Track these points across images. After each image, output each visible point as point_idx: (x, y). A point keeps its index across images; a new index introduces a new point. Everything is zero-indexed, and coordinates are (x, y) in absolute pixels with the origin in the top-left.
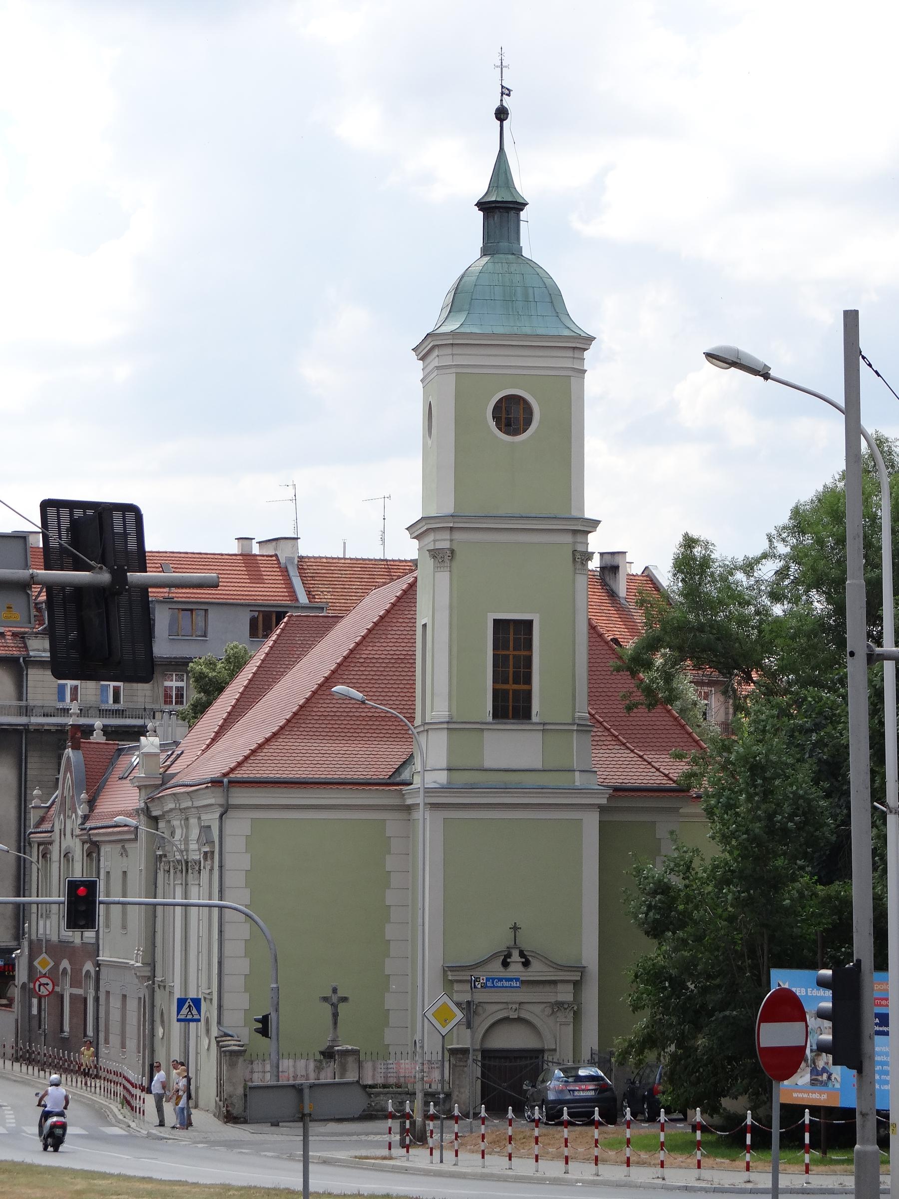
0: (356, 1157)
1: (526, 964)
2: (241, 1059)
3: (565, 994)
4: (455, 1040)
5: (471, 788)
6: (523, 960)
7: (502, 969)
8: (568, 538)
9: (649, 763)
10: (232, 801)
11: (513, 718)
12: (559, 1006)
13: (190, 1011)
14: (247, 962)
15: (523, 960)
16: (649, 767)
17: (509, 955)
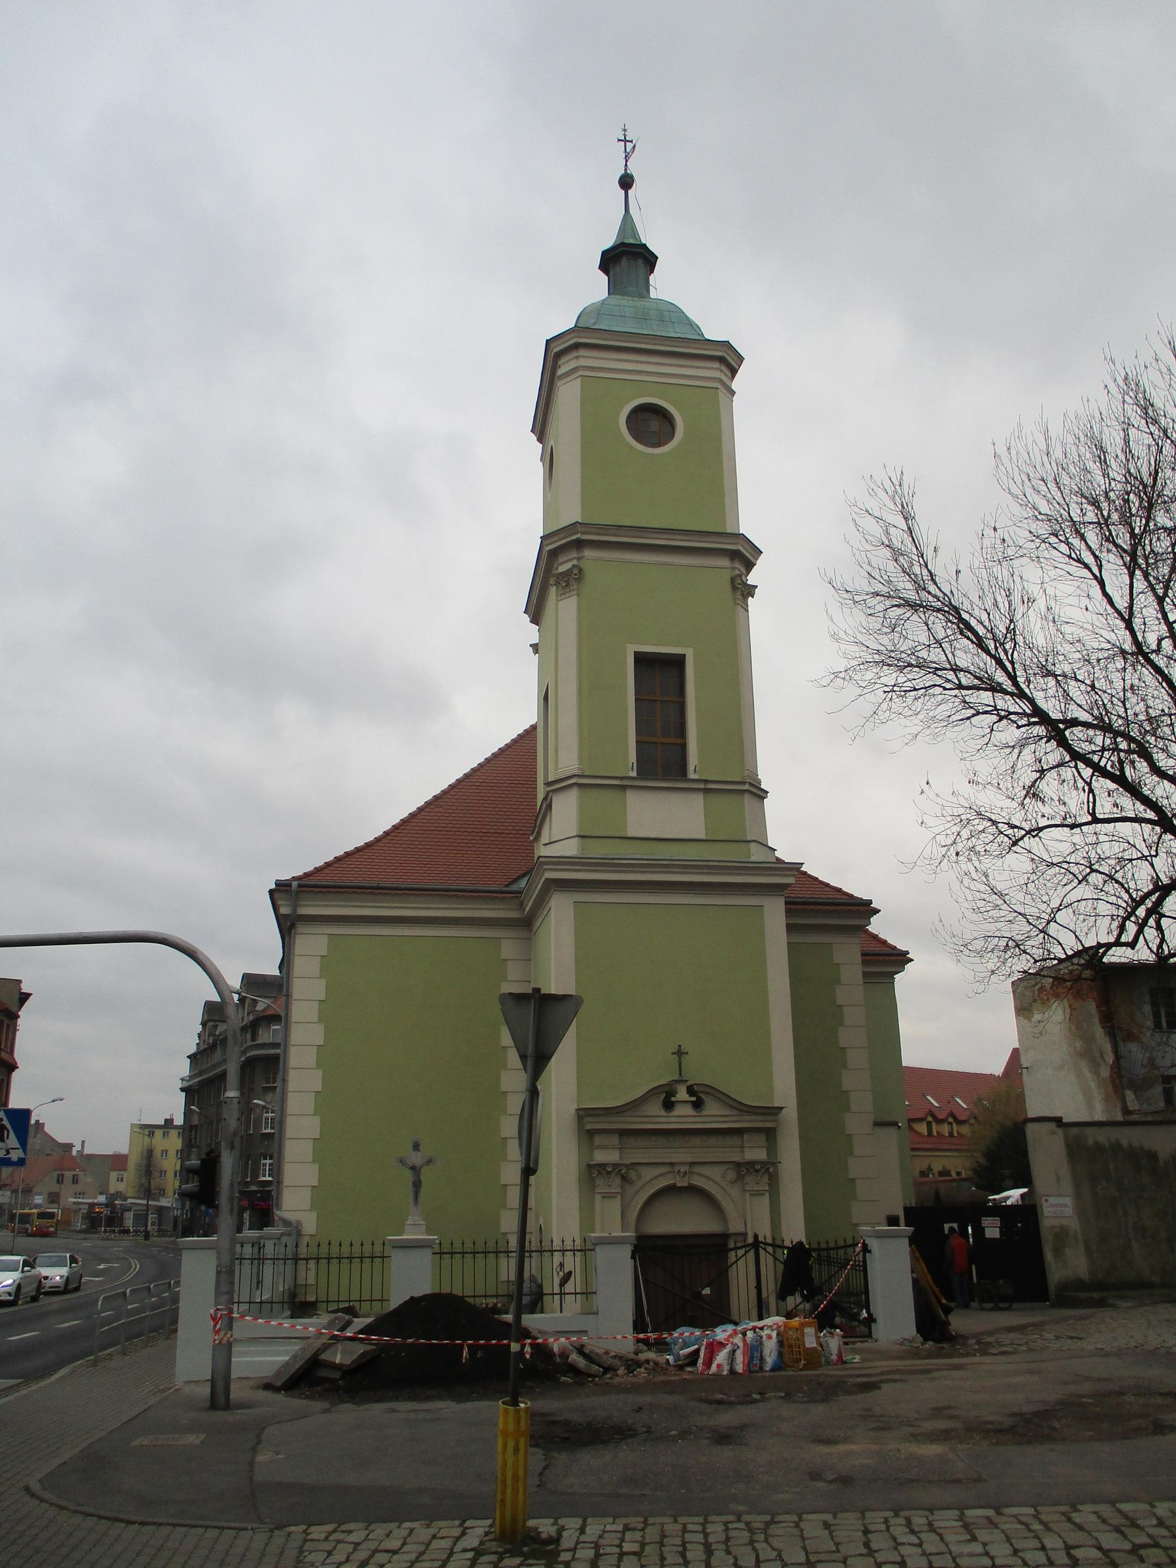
0: (1080, 1339)
3: (756, 1153)
4: (598, 1227)
6: (694, 1099)
7: (663, 1113)
12: (744, 1169)
14: (317, 1121)
15: (694, 1099)
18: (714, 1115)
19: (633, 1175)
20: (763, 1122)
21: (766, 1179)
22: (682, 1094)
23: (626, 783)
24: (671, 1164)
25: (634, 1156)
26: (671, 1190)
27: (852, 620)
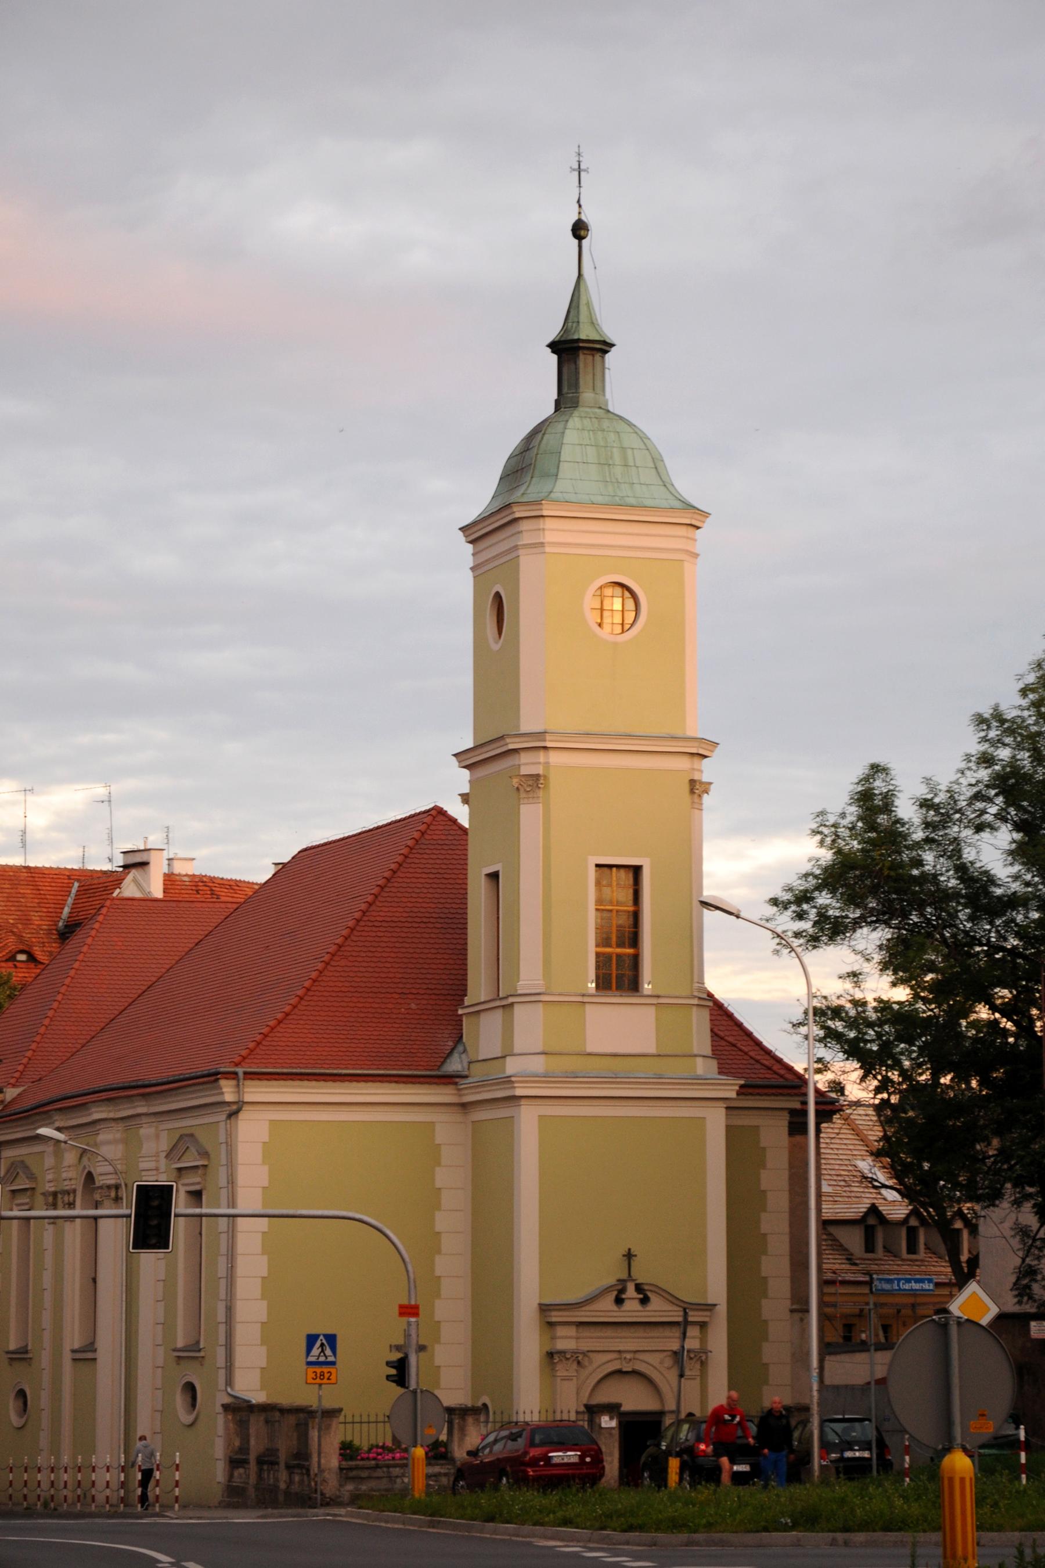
1: (645, 1301)
2: (335, 1421)
5: (571, 1077)
6: (641, 1296)
7: (615, 1308)
8: (683, 764)
9: (746, 1053)
10: (248, 1098)
11: (617, 989)
13: (323, 1351)
15: (641, 1296)
16: (746, 1057)
17: (622, 1291)
18: (659, 1309)
19: (586, 1362)
20: (690, 1317)
21: (698, 1366)
22: (631, 1291)
23: (586, 999)
24: (619, 1352)
25: (585, 1345)
26: (619, 1372)
27: (709, 1348)
